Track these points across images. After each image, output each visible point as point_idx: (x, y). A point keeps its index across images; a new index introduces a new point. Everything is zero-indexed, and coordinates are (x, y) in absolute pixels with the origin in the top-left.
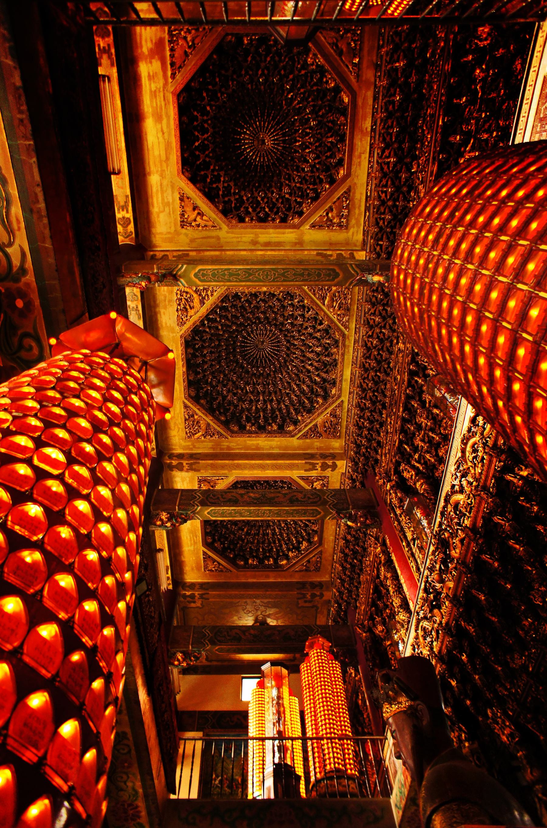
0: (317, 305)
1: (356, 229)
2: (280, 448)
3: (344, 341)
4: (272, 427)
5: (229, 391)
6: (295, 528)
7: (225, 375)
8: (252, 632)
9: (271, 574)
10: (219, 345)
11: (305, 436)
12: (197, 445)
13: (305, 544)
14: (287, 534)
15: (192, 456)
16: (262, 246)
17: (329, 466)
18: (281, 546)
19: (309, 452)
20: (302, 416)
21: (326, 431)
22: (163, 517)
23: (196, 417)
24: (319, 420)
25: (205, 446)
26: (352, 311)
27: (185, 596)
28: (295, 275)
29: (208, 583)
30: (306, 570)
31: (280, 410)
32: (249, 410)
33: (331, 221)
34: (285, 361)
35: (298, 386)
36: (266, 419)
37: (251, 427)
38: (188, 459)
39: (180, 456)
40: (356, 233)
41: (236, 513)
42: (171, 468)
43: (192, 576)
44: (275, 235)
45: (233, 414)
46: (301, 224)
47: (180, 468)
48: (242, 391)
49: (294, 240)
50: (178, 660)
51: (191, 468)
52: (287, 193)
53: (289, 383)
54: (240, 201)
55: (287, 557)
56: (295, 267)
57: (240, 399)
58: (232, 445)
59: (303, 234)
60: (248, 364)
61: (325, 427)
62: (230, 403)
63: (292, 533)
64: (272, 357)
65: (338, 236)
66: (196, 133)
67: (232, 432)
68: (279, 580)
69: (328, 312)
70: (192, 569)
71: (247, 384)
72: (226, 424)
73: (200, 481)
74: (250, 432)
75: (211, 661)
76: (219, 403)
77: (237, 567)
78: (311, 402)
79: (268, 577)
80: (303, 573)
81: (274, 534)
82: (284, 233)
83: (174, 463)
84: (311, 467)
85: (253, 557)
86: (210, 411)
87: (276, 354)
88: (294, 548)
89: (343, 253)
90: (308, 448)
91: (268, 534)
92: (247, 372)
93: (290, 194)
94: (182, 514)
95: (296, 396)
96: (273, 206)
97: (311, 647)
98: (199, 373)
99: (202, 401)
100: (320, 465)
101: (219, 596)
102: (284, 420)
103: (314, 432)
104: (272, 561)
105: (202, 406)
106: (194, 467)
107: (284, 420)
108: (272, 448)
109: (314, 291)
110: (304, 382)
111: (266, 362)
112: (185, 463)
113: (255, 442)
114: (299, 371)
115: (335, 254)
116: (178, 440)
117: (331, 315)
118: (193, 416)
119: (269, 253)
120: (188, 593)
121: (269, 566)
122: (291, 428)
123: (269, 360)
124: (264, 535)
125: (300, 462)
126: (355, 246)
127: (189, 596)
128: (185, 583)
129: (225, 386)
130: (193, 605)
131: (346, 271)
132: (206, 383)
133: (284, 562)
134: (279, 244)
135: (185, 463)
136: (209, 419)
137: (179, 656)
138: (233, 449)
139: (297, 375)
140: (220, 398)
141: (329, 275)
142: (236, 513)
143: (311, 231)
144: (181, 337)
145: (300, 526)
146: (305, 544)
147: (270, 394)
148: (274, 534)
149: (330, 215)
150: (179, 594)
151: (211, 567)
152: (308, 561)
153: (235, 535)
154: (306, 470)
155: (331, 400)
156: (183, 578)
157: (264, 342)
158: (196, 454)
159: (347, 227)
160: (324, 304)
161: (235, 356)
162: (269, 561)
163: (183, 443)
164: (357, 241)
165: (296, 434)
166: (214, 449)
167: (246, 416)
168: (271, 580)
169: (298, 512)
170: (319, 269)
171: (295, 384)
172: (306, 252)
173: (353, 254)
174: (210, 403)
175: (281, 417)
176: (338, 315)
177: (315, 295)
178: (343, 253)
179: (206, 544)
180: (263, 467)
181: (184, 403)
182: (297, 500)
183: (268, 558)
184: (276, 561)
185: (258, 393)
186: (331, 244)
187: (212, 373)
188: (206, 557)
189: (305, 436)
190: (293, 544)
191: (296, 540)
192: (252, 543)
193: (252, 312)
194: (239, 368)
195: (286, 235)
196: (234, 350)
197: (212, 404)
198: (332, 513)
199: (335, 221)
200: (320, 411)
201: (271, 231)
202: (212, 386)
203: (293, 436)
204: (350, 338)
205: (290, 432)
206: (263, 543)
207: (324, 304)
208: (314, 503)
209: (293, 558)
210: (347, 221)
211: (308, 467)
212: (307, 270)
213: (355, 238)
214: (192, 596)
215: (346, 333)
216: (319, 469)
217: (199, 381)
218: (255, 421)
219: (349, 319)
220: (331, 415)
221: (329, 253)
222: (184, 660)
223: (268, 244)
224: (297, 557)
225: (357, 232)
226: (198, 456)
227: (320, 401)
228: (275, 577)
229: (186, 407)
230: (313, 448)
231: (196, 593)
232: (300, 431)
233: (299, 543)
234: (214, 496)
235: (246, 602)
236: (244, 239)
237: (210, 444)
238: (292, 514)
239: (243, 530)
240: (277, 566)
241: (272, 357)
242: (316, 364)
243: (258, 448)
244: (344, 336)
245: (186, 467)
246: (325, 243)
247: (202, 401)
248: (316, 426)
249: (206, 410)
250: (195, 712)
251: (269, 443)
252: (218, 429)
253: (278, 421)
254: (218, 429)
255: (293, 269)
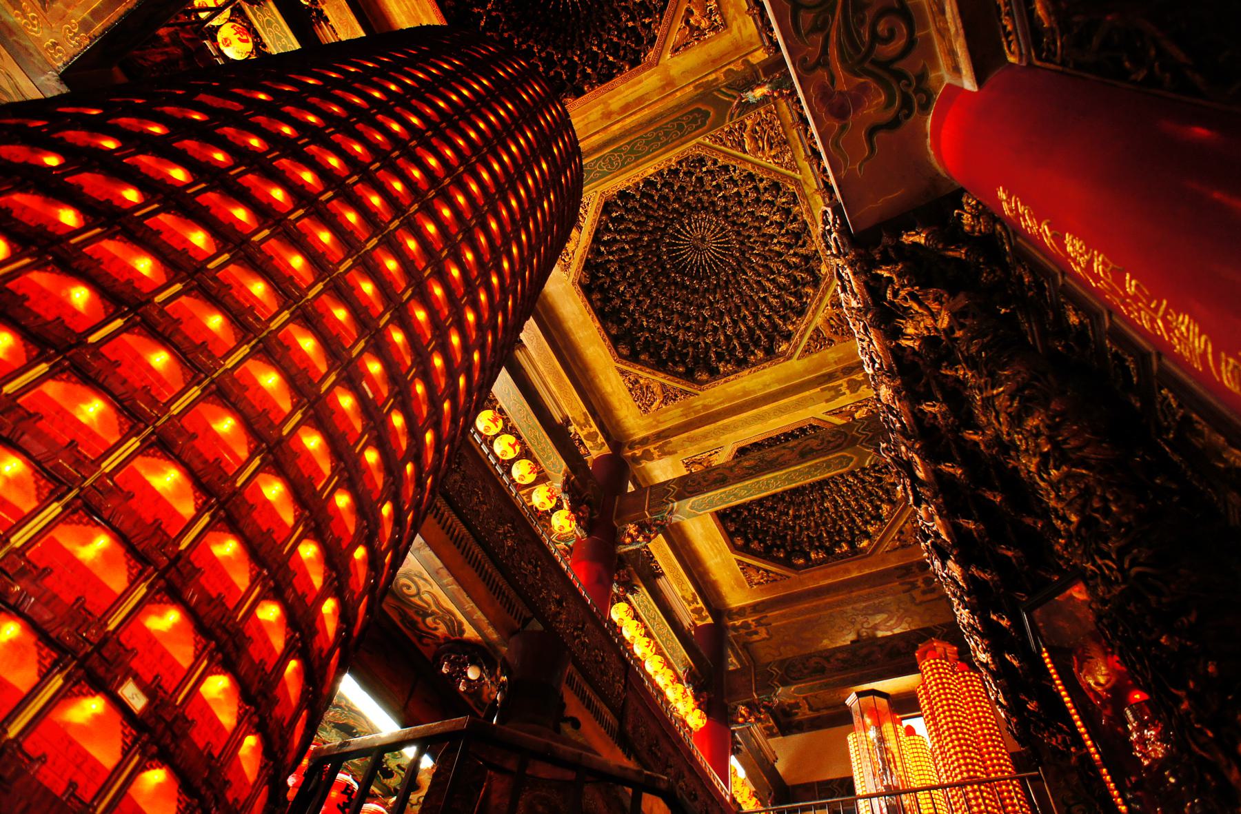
0: (736, 157)
1: (740, 20)
2: (779, 381)
3: (801, 189)
4: (755, 355)
5: (677, 328)
6: (864, 488)
7: (664, 309)
8: (840, 656)
9: (848, 565)
10: (637, 271)
11: (807, 351)
12: (661, 418)
13: (885, 508)
14: (856, 500)
15: (660, 436)
16: (619, 114)
17: (861, 383)
18: (853, 521)
19: (824, 371)
20: (793, 323)
21: (836, 333)
22: (632, 531)
23: (642, 381)
24: (819, 320)
25: (673, 415)
26: (791, 140)
27: (735, 628)
28: (647, 143)
29: (763, 602)
30: (903, 546)
31: (761, 327)
32: (716, 344)
33: (698, 28)
34: (743, 253)
35: (773, 281)
36: (745, 347)
37: (725, 366)
38: (655, 442)
39: (644, 441)
40: (746, 27)
41: (727, 497)
42: (636, 460)
43: (736, 596)
44: (631, 90)
45: (696, 359)
46: (659, 55)
47: (648, 456)
48: (696, 319)
49: (659, 84)
50: (742, 716)
51: (664, 454)
52: (627, 21)
53: (758, 283)
54: (572, 67)
55: (867, 535)
56: (641, 133)
57: (697, 334)
58: (707, 402)
59: (667, 68)
60: (692, 278)
61: (832, 326)
62: (685, 344)
63: (863, 498)
64: (723, 255)
65: (718, 44)
66: (476, 10)
67: (701, 383)
68: (867, 571)
69: (757, 160)
70: (733, 588)
71: (702, 306)
72: (689, 376)
73: (687, 466)
74: (727, 374)
75: (818, 710)
76: (670, 349)
77: (797, 568)
78: (798, 295)
79: (847, 571)
80: (898, 552)
81: (836, 505)
82: (640, 82)
83: (638, 452)
84: (833, 393)
85: (816, 548)
86: (659, 365)
87: (726, 249)
88: (873, 518)
89: (731, 67)
90: (822, 366)
91: (827, 510)
92: (695, 291)
93: (633, 19)
94: (656, 520)
95: (775, 297)
96: (615, 49)
97: (924, 657)
98: (625, 320)
99: (642, 357)
100: (845, 385)
101: (783, 616)
102: (771, 339)
103: (819, 340)
104: (845, 547)
105: (645, 364)
106: (666, 449)
107: (771, 339)
108: (766, 386)
109: (721, 140)
110: (779, 273)
111: (717, 266)
112: (651, 448)
113: (738, 387)
114: (766, 259)
115: (720, 75)
116: (633, 420)
117: (763, 163)
118: (637, 382)
119: (628, 121)
120: (738, 623)
121: (843, 556)
122: (784, 347)
123: (721, 261)
124: (821, 512)
125: (812, 391)
126: (751, 44)
127: (742, 626)
128: (730, 611)
129: (669, 323)
130: (756, 637)
131: (717, 103)
132: (642, 328)
133: (865, 543)
134: (640, 100)
135: (651, 448)
136: (660, 378)
137: (743, 710)
138: (713, 406)
139: (766, 267)
140: (668, 343)
141: (695, 120)
142: (727, 497)
143: (676, 59)
144: (573, 284)
145: (870, 483)
146: (885, 508)
147: (738, 308)
148: (836, 505)
149: (692, 21)
150: (727, 627)
151: (756, 578)
152: (901, 532)
153: (777, 524)
154: (827, 401)
155: (823, 286)
156: (725, 605)
157: (703, 236)
158: (663, 431)
159: (725, 25)
160: (745, 152)
161: (668, 277)
162: (841, 547)
163: (642, 422)
164: (751, 35)
165: (793, 354)
166: (686, 415)
167: (716, 353)
168: (855, 574)
169: (816, 467)
170: (676, 120)
171: (768, 280)
172: (678, 94)
173: (748, 61)
174: (655, 354)
175: (766, 336)
176: (774, 157)
177: (724, 145)
178: (731, 67)
179: (735, 548)
180: (761, 418)
181: (618, 369)
182: (812, 450)
183: (838, 544)
184: (851, 544)
185: (722, 314)
186: (714, 61)
187: (645, 314)
188: (745, 567)
189: (807, 351)
190: (869, 513)
191: (872, 505)
192: (808, 528)
193: (678, 200)
194: (680, 290)
195: (645, 82)
196: (664, 268)
197: (660, 356)
198: (869, 454)
199: (703, 25)
200: (813, 306)
201: (622, 87)
202: (650, 330)
203: (790, 358)
204: (809, 182)
205: (784, 353)
206: (825, 524)
207: (745, 152)
208: (838, 448)
209: (876, 533)
210: (721, 15)
211: (828, 394)
212: (661, 128)
213: (746, 33)
214: (746, 625)
215: (799, 176)
216: (848, 392)
217: (630, 330)
218: (730, 355)
219: (793, 156)
220: (832, 306)
221: (713, 76)
222: (750, 714)
223: (626, 108)
224: (880, 530)
225: (744, 23)
226: (667, 433)
227: (810, 291)
228: (859, 568)
229: (622, 373)
230: (829, 365)
231: (750, 620)
232: (796, 347)
233: (878, 508)
234: (693, 481)
235: (831, 615)
236: (592, 118)
237: (679, 411)
238: (809, 472)
239: (787, 514)
240: (855, 551)
241: (723, 255)
242: (783, 240)
243: (746, 393)
244: (797, 182)
245: (656, 453)
246: (705, 64)
247: (642, 357)
248: (817, 330)
249: (652, 367)
250: (813, 783)
251: (759, 380)
252: (679, 386)
253: (765, 343)
254: (679, 386)
255: (641, 137)
